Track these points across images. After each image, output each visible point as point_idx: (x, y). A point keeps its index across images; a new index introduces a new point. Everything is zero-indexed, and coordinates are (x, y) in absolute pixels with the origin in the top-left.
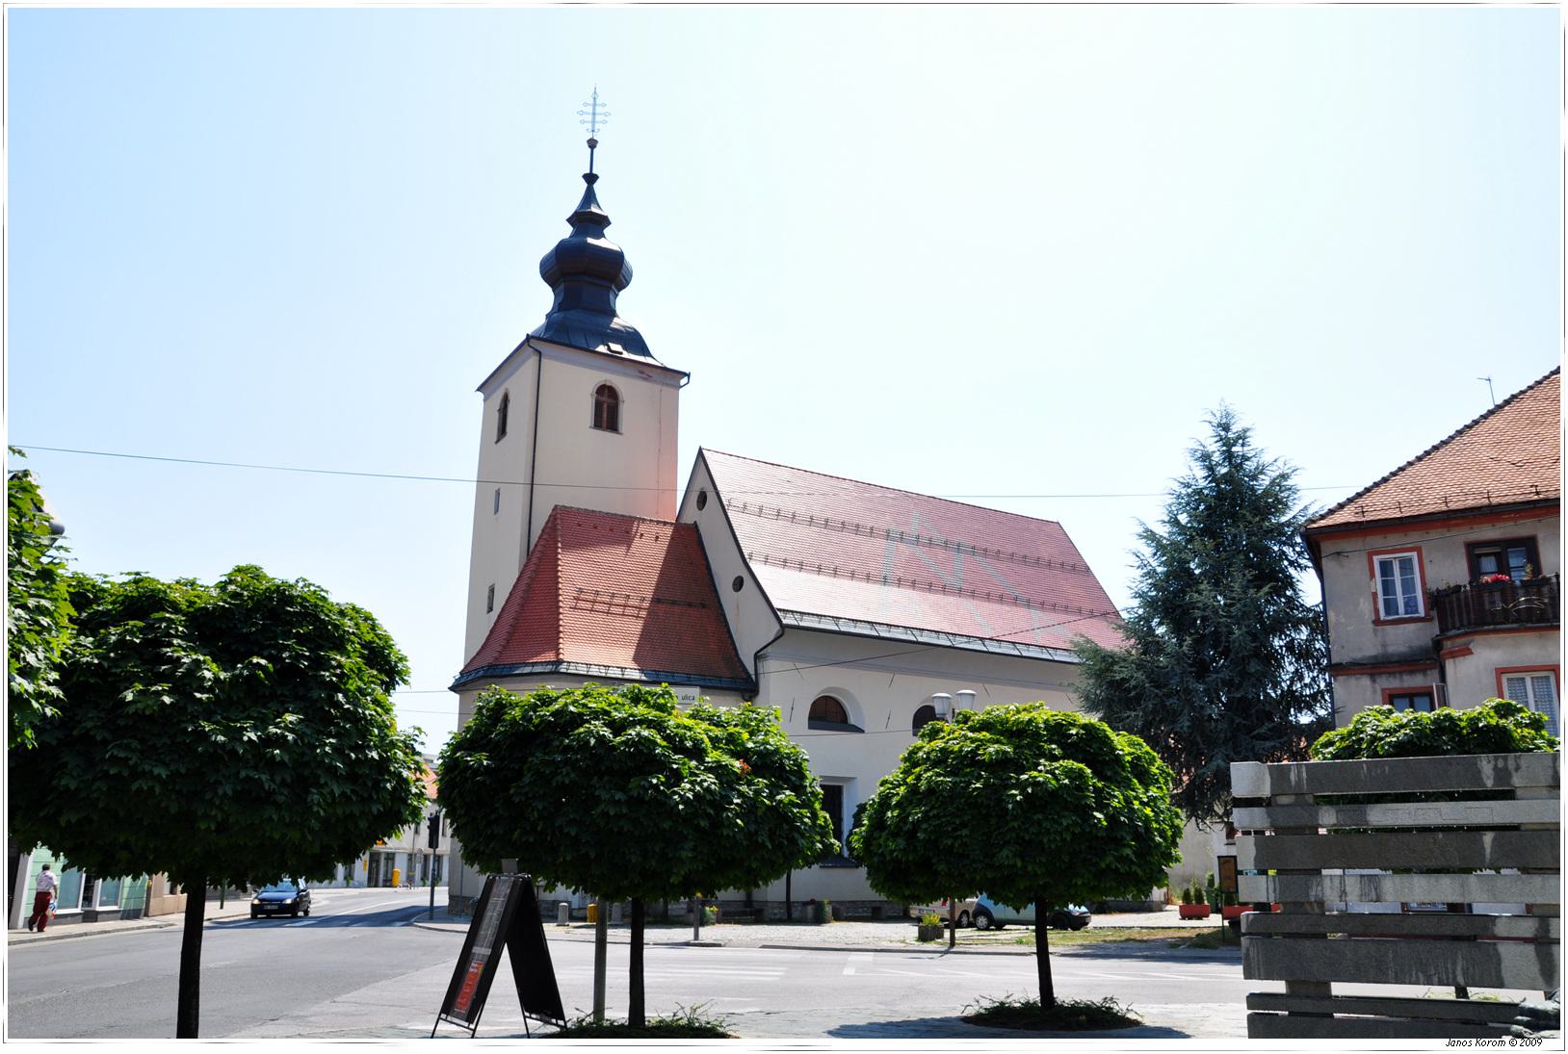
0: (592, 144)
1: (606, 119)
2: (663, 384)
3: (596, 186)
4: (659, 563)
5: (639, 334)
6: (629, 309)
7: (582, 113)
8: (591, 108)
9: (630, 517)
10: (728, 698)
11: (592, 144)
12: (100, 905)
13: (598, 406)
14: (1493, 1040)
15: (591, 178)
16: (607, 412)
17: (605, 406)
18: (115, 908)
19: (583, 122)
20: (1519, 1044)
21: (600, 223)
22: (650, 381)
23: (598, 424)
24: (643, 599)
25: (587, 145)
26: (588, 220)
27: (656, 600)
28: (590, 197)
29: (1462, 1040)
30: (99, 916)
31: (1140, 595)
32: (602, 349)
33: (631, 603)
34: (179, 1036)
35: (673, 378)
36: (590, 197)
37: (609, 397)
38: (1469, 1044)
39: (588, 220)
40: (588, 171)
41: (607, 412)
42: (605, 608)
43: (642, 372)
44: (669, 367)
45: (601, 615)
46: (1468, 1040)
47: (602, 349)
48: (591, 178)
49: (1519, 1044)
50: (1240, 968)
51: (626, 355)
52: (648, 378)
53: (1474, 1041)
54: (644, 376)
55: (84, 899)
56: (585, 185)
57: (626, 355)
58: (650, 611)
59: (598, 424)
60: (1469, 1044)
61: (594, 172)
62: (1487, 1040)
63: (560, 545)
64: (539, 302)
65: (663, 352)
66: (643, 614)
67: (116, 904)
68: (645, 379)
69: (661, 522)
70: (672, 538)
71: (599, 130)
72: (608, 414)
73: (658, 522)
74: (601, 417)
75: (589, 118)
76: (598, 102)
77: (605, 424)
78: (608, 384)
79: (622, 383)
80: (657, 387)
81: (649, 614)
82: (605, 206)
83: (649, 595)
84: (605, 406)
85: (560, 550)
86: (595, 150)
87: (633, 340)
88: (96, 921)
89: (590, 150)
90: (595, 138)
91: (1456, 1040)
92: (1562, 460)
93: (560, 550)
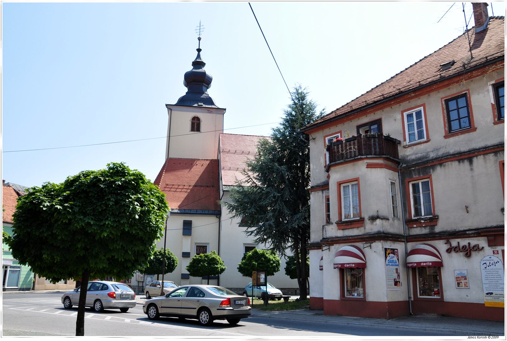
0: (199, 39)
1: (204, 30)
2: (216, 113)
3: (201, 53)
4: (200, 174)
5: (211, 98)
6: (211, 92)
7: (196, 30)
8: (199, 27)
9: (194, 159)
10: (212, 217)
11: (199, 39)
12: (7, 286)
13: (193, 124)
14: (483, 336)
15: (199, 50)
16: (196, 125)
17: (196, 123)
18: (17, 287)
19: (197, 32)
20: (491, 338)
21: (202, 64)
22: (212, 113)
23: (193, 130)
24: (190, 186)
25: (198, 39)
26: (198, 64)
27: (195, 186)
28: (199, 56)
29: (473, 337)
30: (6, 290)
31: (410, 159)
32: (196, 105)
33: (185, 187)
34: (77, 335)
35: (222, 111)
36: (199, 56)
37: (197, 120)
38: (475, 338)
39: (198, 64)
40: (198, 48)
41: (196, 125)
42: (169, 189)
43: (209, 111)
44: (220, 108)
45: (179, 193)
46: (475, 336)
47: (196, 105)
48: (199, 50)
49: (491, 338)
50: (324, 299)
51: (204, 106)
52: (211, 112)
53: (477, 337)
54: (209, 112)
55: (29, 290)
56: (197, 52)
57: (204, 106)
58: (192, 190)
59: (193, 130)
60: (475, 338)
61: (200, 48)
62: (481, 336)
63: (164, 171)
64: (183, 91)
65: (218, 103)
66: (189, 191)
67: (17, 286)
68: (210, 113)
69: (206, 160)
70: (208, 165)
71: (201, 34)
72: (197, 126)
73: (204, 160)
74: (194, 127)
75: (198, 31)
76: (201, 25)
77: (195, 130)
78: (196, 116)
79: (200, 115)
80: (215, 115)
81: (191, 191)
82: (203, 59)
83: (193, 183)
84: (196, 123)
85: (164, 172)
86: (200, 41)
87: (209, 101)
88: (5, 291)
89: (199, 41)
90: (200, 37)
91: (471, 336)
92: (505, 51)
93: (164, 172)
